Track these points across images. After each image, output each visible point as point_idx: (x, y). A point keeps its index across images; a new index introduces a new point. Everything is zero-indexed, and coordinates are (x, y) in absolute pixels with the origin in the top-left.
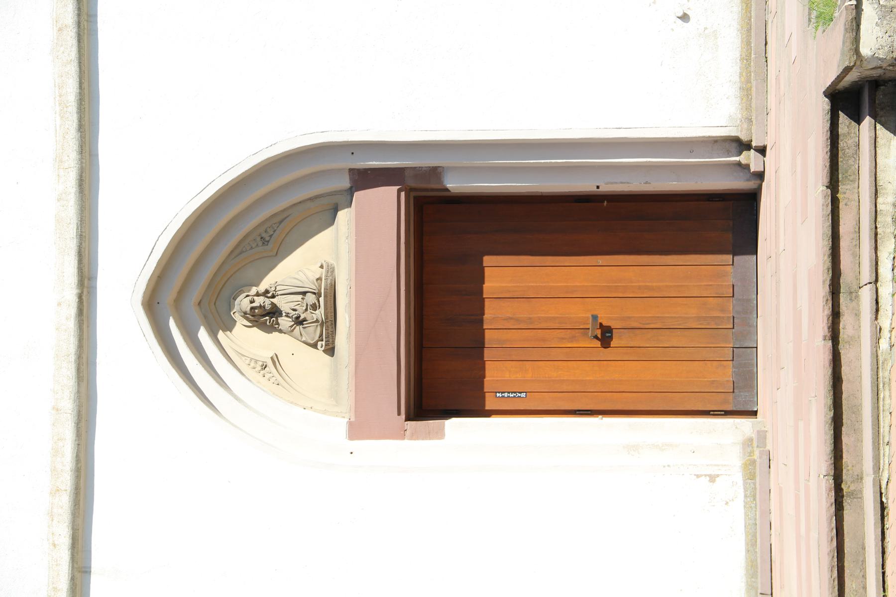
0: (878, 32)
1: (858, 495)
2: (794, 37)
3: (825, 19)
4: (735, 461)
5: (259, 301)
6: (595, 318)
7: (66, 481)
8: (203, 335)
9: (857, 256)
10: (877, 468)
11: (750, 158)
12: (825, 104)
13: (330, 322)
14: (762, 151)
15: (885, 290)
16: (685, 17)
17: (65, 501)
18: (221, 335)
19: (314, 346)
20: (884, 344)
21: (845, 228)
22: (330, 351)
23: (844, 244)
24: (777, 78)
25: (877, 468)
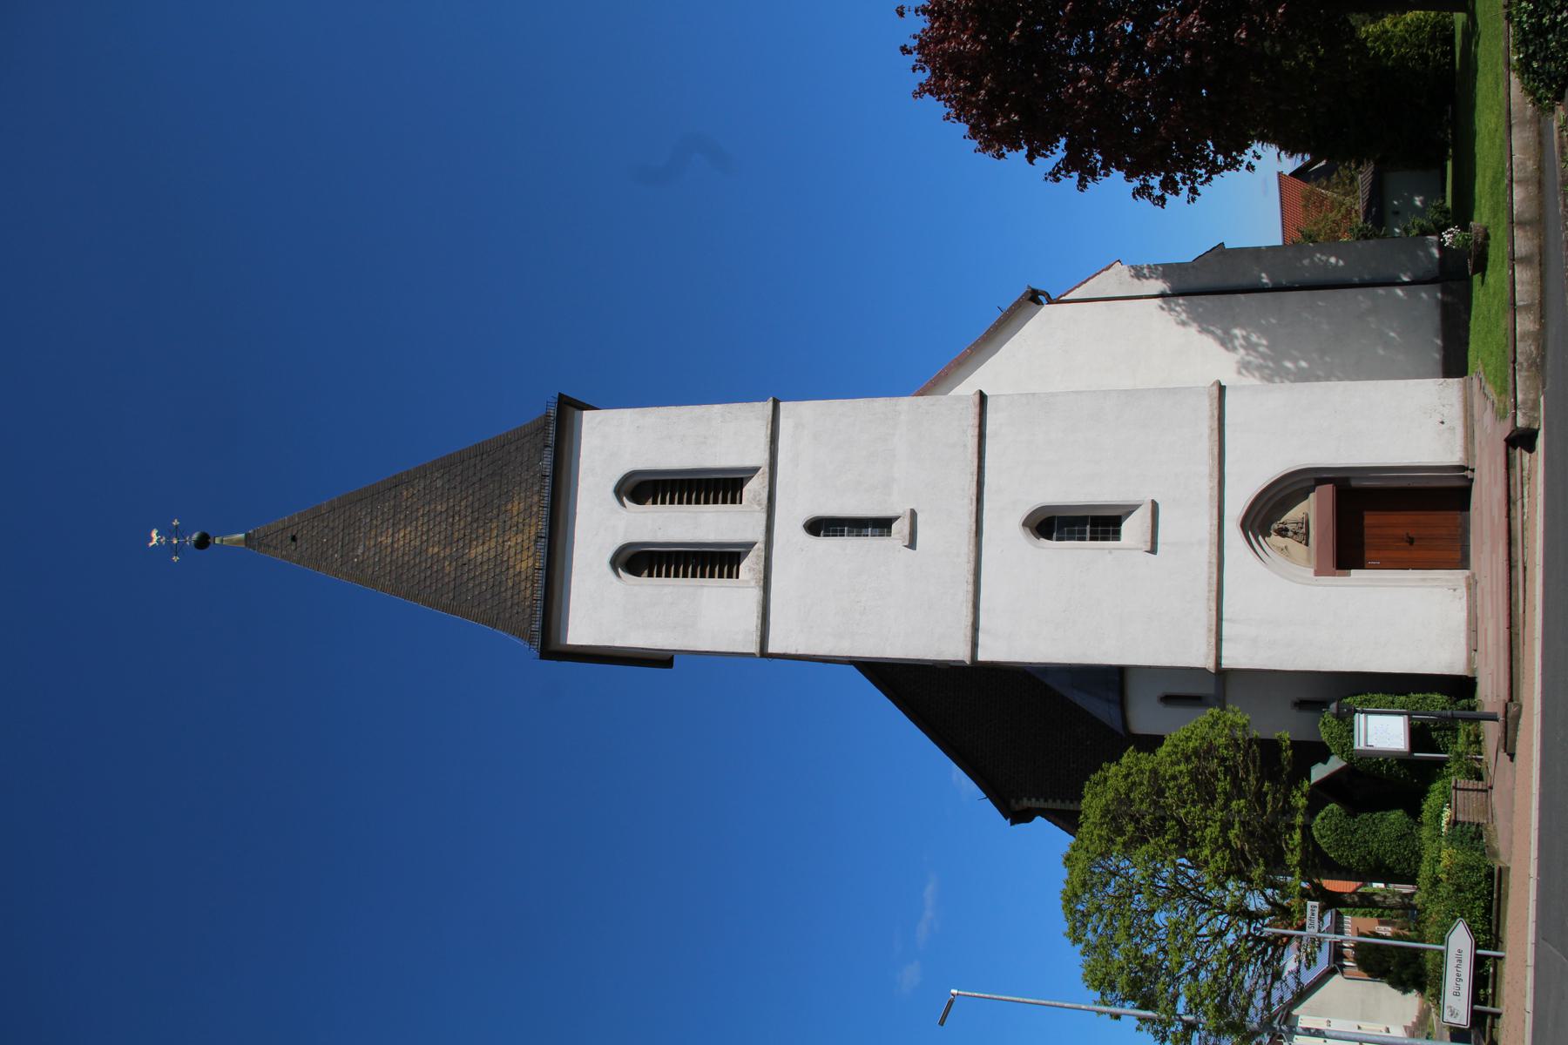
0: (1522, 420)
1: (1516, 567)
2: (1489, 427)
3: (1504, 417)
4: (1463, 584)
5: (1281, 526)
6: (1407, 534)
7: (1214, 587)
8: (1260, 538)
9: (1516, 493)
10: (1523, 555)
11: (1468, 473)
12: (1503, 444)
13: (1307, 534)
14: (1473, 470)
15: (1526, 500)
16: (1442, 423)
17: (1214, 594)
18: (1266, 538)
19: (1301, 542)
20: (1525, 517)
21: (1512, 482)
22: (1307, 544)
23: (1512, 487)
24: (1480, 443)
25: (1523, 555)
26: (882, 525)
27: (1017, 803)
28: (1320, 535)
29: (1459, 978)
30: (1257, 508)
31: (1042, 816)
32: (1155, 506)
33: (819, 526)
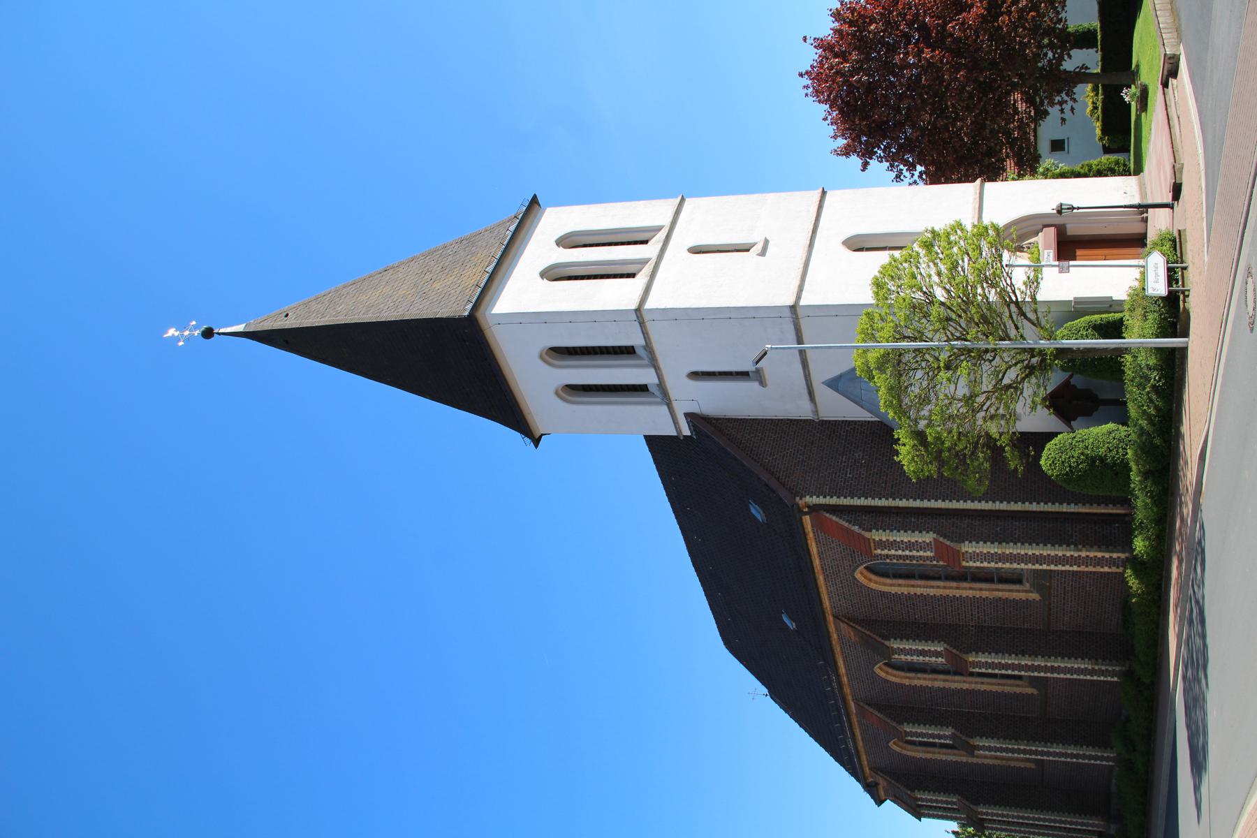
26: (745, 249)
27: (801, 499)
29: (1157, 275)
33: (697, 250)
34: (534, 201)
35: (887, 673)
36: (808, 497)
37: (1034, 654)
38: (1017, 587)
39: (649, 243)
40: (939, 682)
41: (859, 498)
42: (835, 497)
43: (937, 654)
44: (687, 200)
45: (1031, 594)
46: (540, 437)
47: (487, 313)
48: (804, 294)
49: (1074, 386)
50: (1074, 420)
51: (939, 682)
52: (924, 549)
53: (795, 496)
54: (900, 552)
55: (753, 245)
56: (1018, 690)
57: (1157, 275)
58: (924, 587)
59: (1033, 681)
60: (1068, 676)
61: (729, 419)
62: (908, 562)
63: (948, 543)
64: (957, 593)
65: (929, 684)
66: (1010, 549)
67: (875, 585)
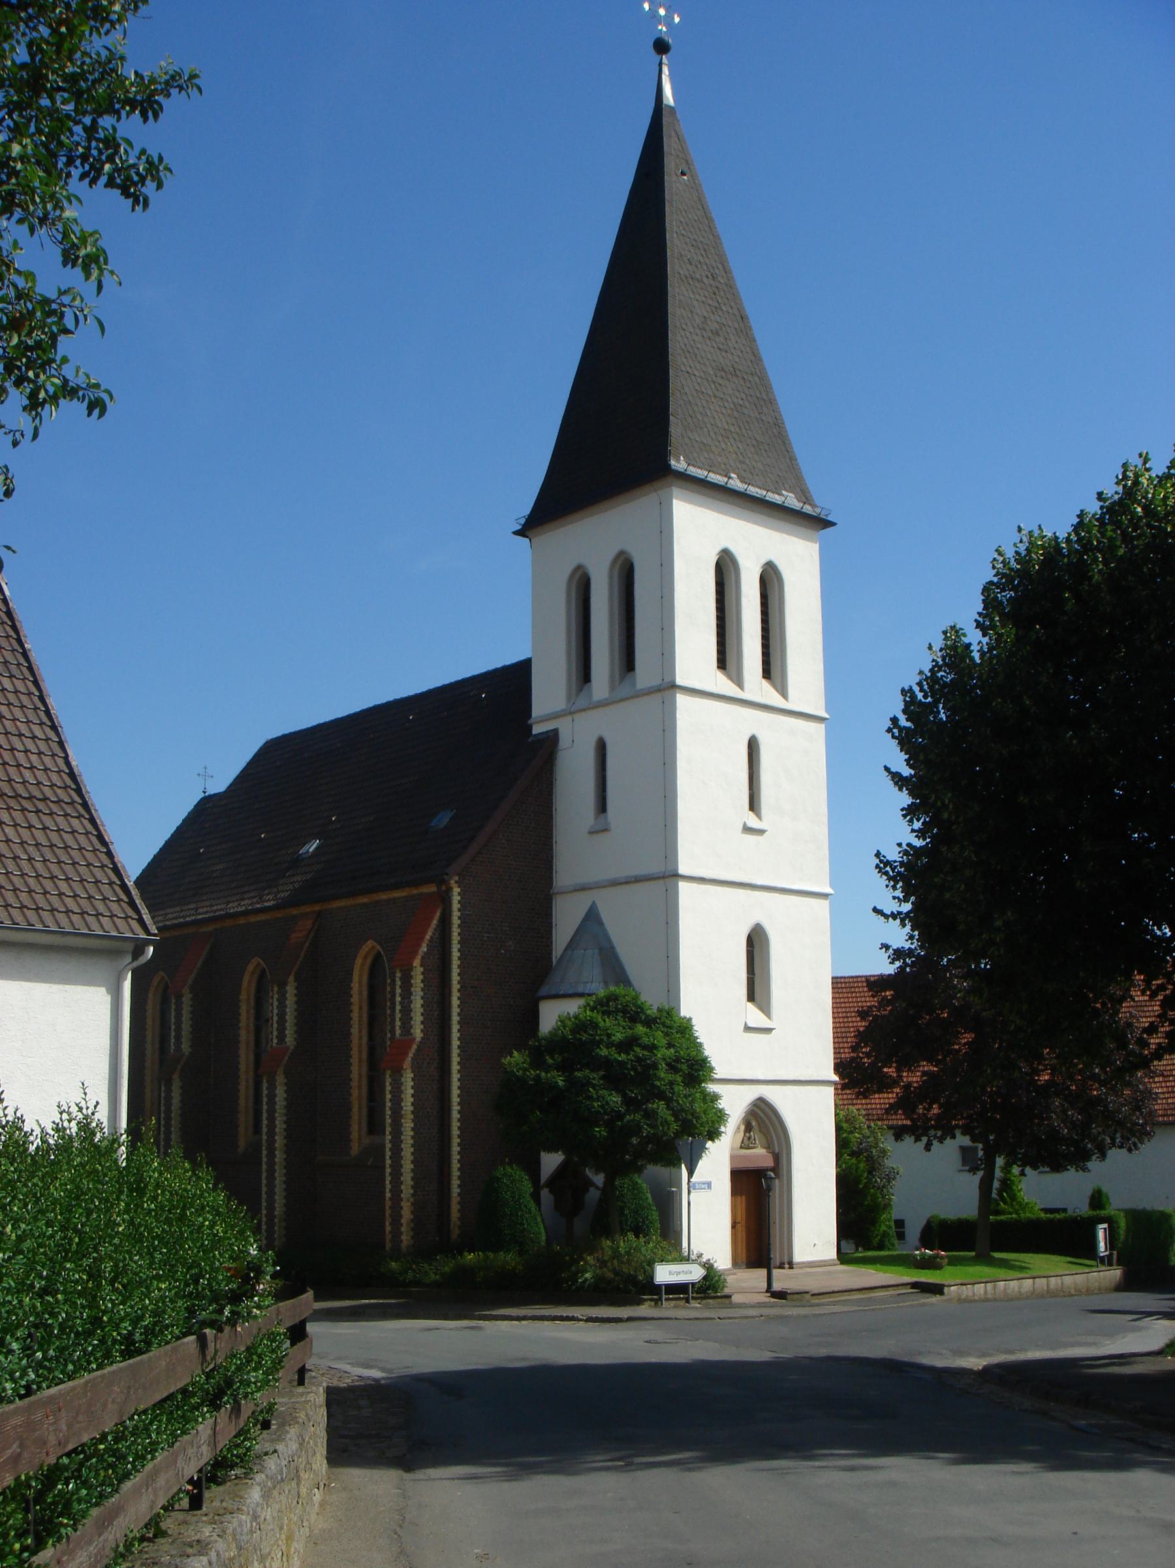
22: (741, 1147)
26: (754, 804)
27: (456, 882)
28: (744, 1156)
29: (678, 1273)
30: (767, 1110)
31: (890, 975)
32: (768, 1030)
33: (753, 746)
34: (826, 524)
35: (253, 973)
36: (459, 890)
37: (288, 1150)
38: (365, 1129)
39: (764, 682)
40: (245, 1035)
41: (459, 950)
42: (459, 922)
43: (281, 1037)
44: (823, 726)
45: (357, 1144)
46: (527, 537)
47: (676, 491)
48: (694, 886)
49: (588, 1190)
50: (550, 1192)
51: (245, 1035)
52: (403, 1027)
53: (458, 874)
54: (398, 999)
55: (759, 816)
56: (241, 1130)
57: (678, 1273)
58: (359, 1021)
59: (257, 1146)
60: (264, 1189)
61: (552, 785)
62: (388, 1004)
63: (411, 1055)
64: (355, 1060)
65: (243, 1024)
66: (408, 1125)
67: (360, 963)
